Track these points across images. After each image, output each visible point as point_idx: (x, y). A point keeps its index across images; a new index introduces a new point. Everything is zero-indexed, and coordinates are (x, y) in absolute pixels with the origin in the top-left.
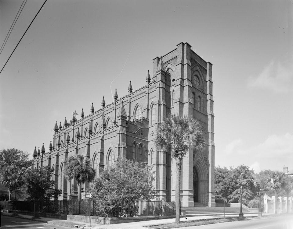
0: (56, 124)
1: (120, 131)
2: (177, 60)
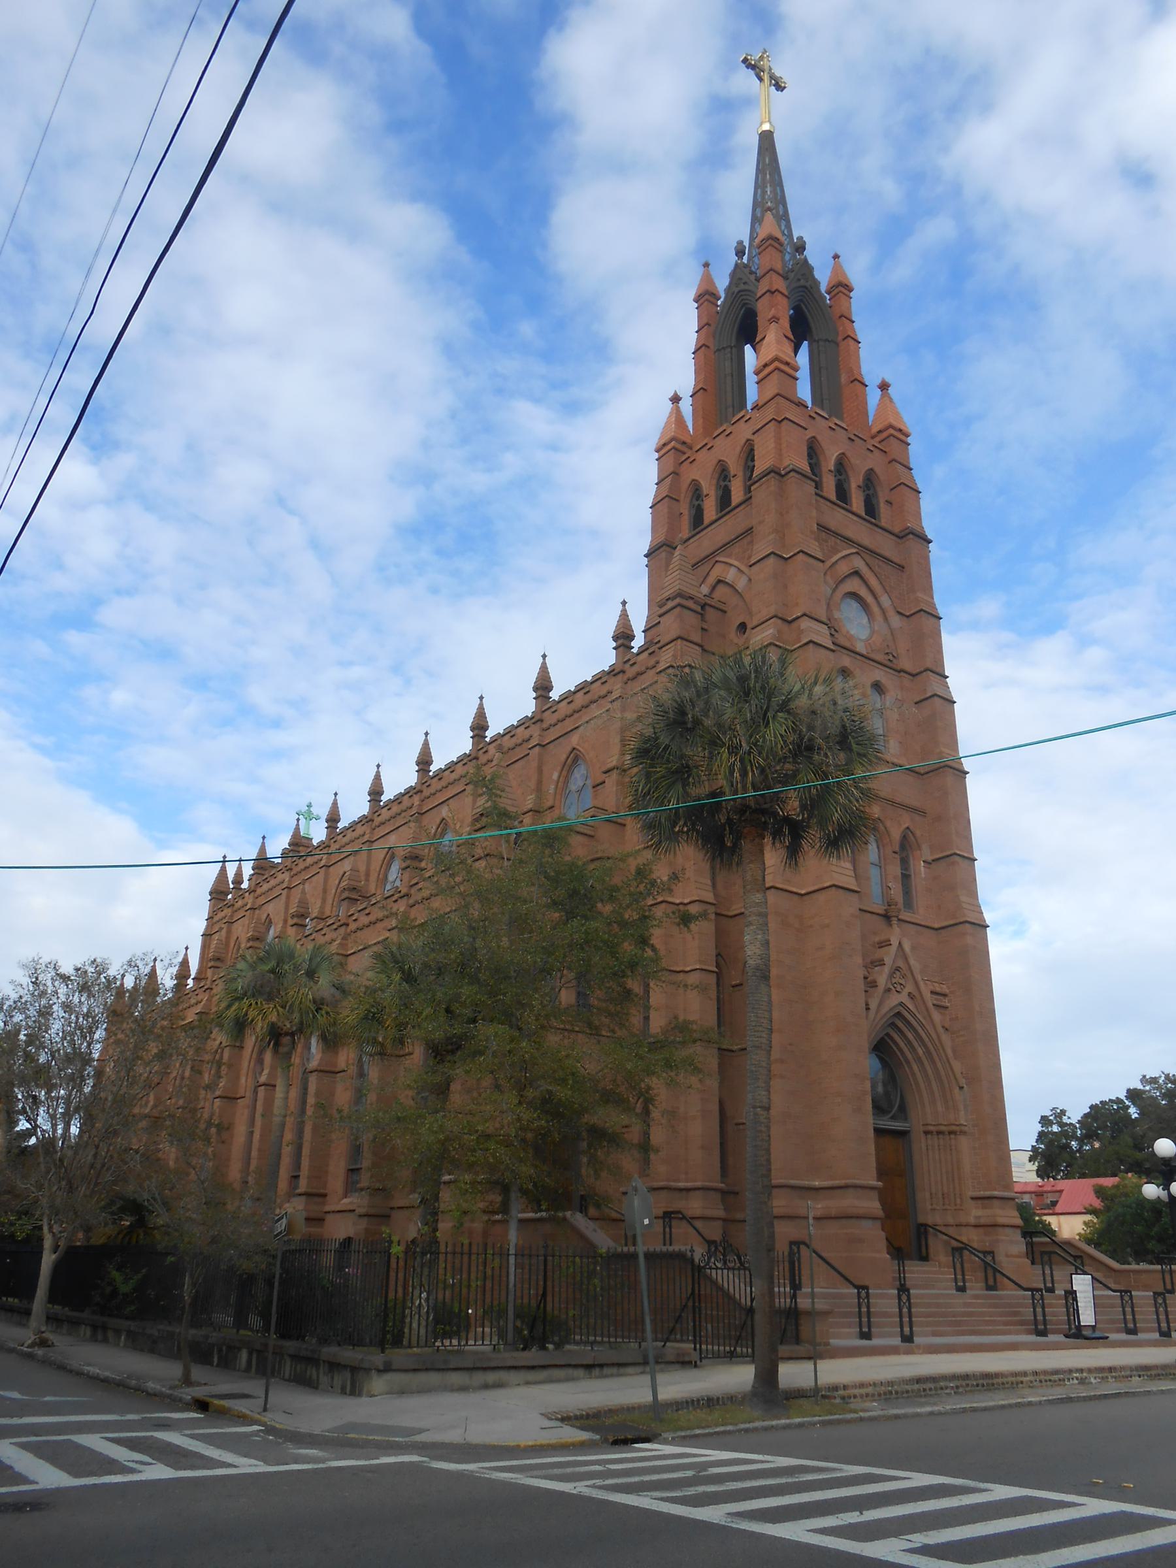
0: (624, 616)
2: (751, 542)
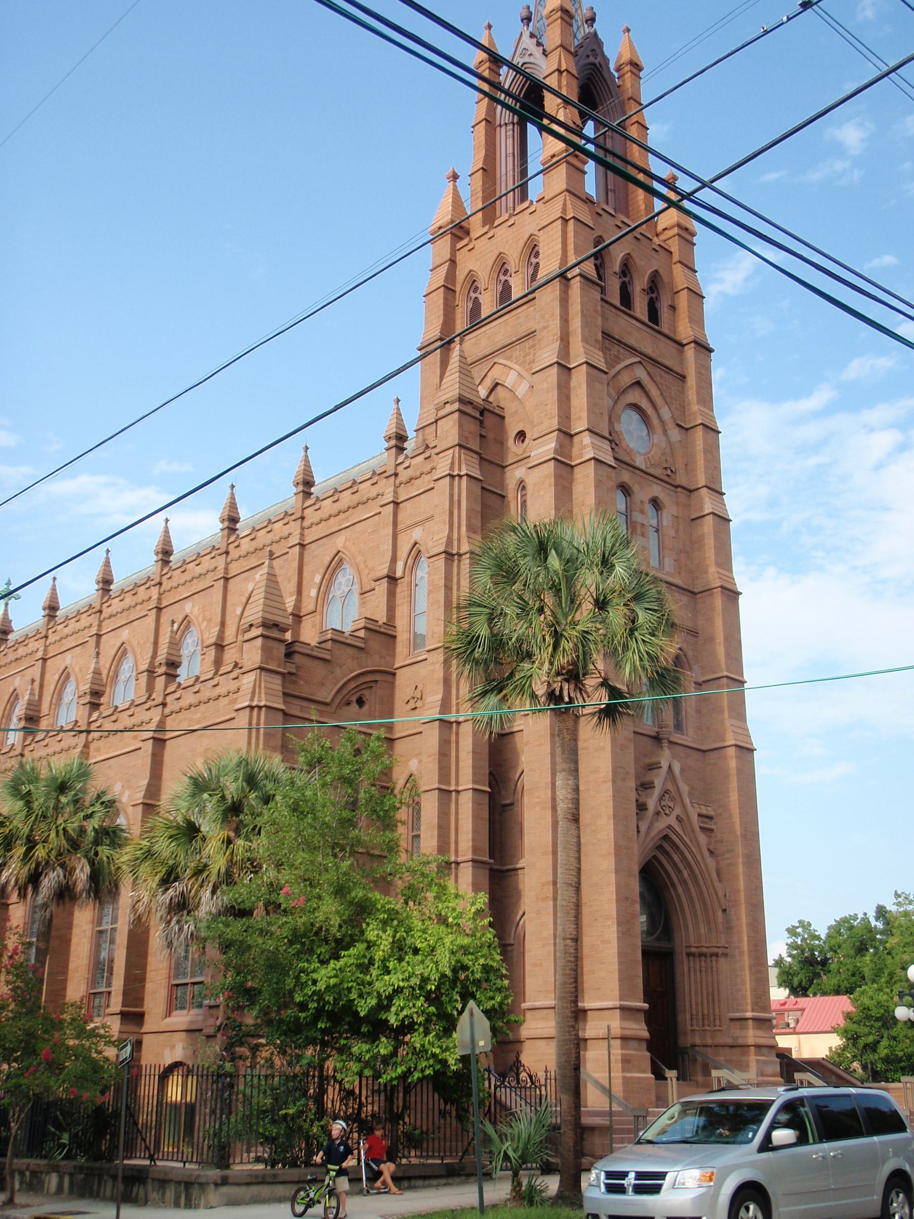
1: (253, 693)
